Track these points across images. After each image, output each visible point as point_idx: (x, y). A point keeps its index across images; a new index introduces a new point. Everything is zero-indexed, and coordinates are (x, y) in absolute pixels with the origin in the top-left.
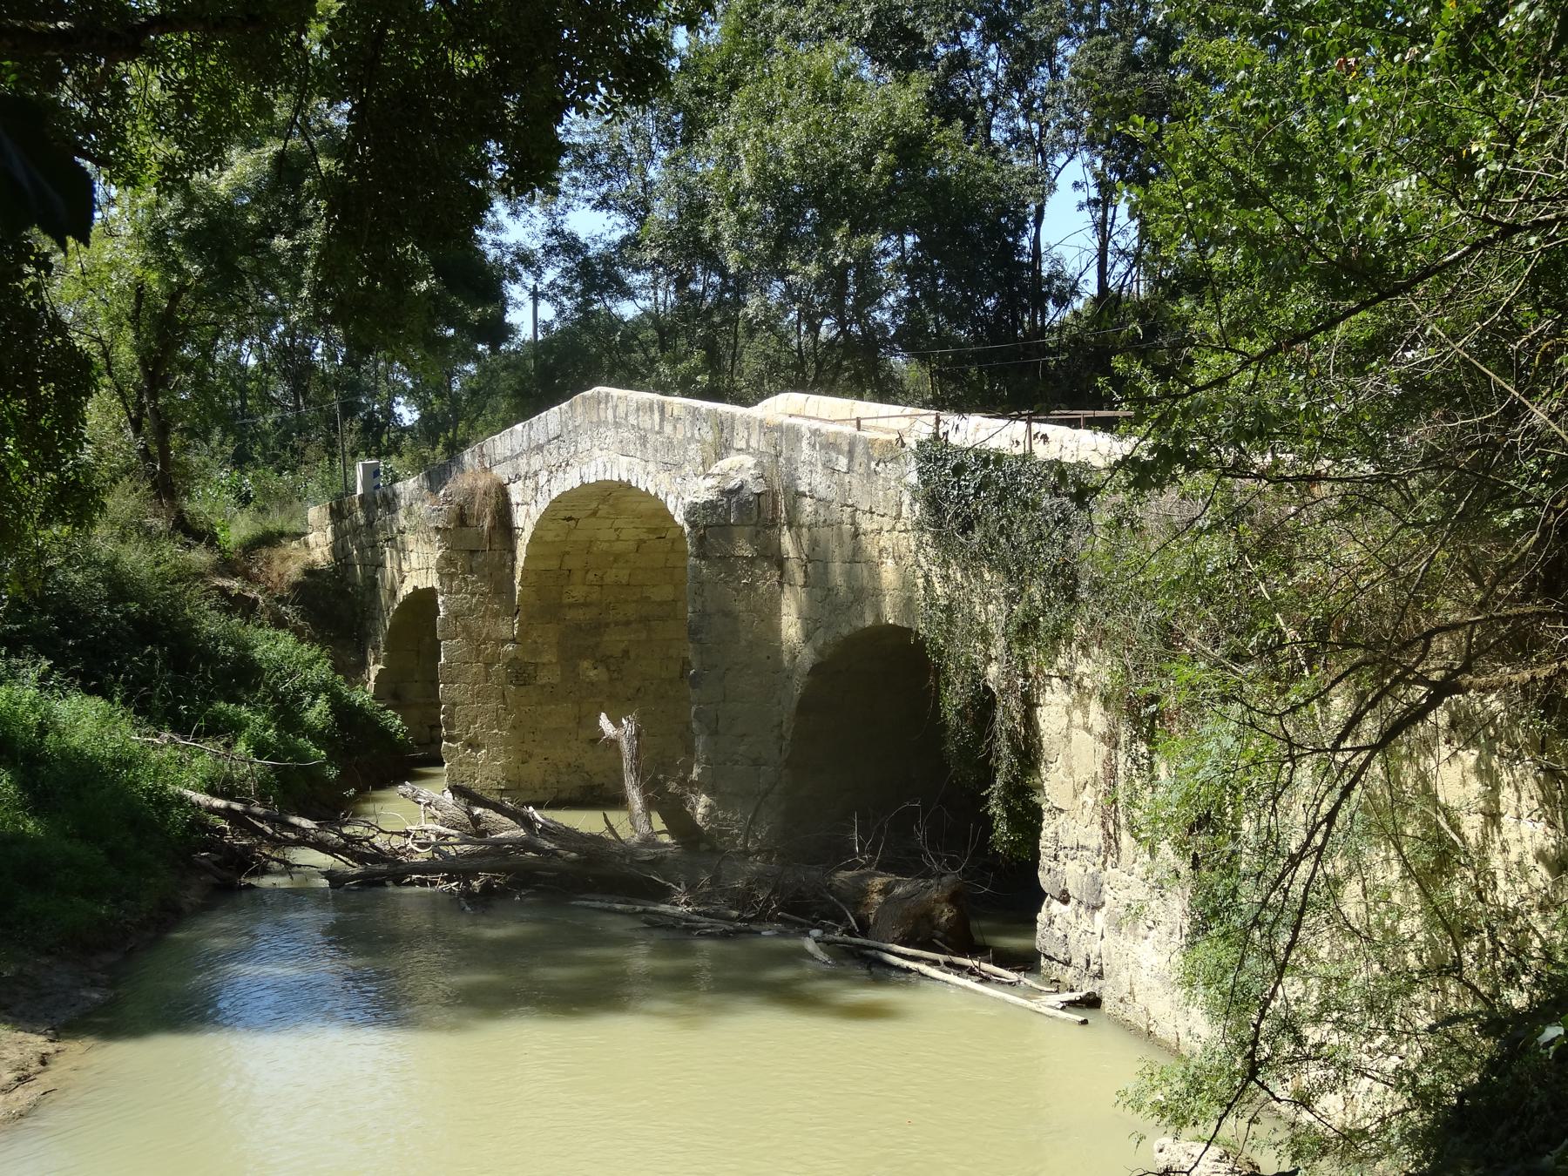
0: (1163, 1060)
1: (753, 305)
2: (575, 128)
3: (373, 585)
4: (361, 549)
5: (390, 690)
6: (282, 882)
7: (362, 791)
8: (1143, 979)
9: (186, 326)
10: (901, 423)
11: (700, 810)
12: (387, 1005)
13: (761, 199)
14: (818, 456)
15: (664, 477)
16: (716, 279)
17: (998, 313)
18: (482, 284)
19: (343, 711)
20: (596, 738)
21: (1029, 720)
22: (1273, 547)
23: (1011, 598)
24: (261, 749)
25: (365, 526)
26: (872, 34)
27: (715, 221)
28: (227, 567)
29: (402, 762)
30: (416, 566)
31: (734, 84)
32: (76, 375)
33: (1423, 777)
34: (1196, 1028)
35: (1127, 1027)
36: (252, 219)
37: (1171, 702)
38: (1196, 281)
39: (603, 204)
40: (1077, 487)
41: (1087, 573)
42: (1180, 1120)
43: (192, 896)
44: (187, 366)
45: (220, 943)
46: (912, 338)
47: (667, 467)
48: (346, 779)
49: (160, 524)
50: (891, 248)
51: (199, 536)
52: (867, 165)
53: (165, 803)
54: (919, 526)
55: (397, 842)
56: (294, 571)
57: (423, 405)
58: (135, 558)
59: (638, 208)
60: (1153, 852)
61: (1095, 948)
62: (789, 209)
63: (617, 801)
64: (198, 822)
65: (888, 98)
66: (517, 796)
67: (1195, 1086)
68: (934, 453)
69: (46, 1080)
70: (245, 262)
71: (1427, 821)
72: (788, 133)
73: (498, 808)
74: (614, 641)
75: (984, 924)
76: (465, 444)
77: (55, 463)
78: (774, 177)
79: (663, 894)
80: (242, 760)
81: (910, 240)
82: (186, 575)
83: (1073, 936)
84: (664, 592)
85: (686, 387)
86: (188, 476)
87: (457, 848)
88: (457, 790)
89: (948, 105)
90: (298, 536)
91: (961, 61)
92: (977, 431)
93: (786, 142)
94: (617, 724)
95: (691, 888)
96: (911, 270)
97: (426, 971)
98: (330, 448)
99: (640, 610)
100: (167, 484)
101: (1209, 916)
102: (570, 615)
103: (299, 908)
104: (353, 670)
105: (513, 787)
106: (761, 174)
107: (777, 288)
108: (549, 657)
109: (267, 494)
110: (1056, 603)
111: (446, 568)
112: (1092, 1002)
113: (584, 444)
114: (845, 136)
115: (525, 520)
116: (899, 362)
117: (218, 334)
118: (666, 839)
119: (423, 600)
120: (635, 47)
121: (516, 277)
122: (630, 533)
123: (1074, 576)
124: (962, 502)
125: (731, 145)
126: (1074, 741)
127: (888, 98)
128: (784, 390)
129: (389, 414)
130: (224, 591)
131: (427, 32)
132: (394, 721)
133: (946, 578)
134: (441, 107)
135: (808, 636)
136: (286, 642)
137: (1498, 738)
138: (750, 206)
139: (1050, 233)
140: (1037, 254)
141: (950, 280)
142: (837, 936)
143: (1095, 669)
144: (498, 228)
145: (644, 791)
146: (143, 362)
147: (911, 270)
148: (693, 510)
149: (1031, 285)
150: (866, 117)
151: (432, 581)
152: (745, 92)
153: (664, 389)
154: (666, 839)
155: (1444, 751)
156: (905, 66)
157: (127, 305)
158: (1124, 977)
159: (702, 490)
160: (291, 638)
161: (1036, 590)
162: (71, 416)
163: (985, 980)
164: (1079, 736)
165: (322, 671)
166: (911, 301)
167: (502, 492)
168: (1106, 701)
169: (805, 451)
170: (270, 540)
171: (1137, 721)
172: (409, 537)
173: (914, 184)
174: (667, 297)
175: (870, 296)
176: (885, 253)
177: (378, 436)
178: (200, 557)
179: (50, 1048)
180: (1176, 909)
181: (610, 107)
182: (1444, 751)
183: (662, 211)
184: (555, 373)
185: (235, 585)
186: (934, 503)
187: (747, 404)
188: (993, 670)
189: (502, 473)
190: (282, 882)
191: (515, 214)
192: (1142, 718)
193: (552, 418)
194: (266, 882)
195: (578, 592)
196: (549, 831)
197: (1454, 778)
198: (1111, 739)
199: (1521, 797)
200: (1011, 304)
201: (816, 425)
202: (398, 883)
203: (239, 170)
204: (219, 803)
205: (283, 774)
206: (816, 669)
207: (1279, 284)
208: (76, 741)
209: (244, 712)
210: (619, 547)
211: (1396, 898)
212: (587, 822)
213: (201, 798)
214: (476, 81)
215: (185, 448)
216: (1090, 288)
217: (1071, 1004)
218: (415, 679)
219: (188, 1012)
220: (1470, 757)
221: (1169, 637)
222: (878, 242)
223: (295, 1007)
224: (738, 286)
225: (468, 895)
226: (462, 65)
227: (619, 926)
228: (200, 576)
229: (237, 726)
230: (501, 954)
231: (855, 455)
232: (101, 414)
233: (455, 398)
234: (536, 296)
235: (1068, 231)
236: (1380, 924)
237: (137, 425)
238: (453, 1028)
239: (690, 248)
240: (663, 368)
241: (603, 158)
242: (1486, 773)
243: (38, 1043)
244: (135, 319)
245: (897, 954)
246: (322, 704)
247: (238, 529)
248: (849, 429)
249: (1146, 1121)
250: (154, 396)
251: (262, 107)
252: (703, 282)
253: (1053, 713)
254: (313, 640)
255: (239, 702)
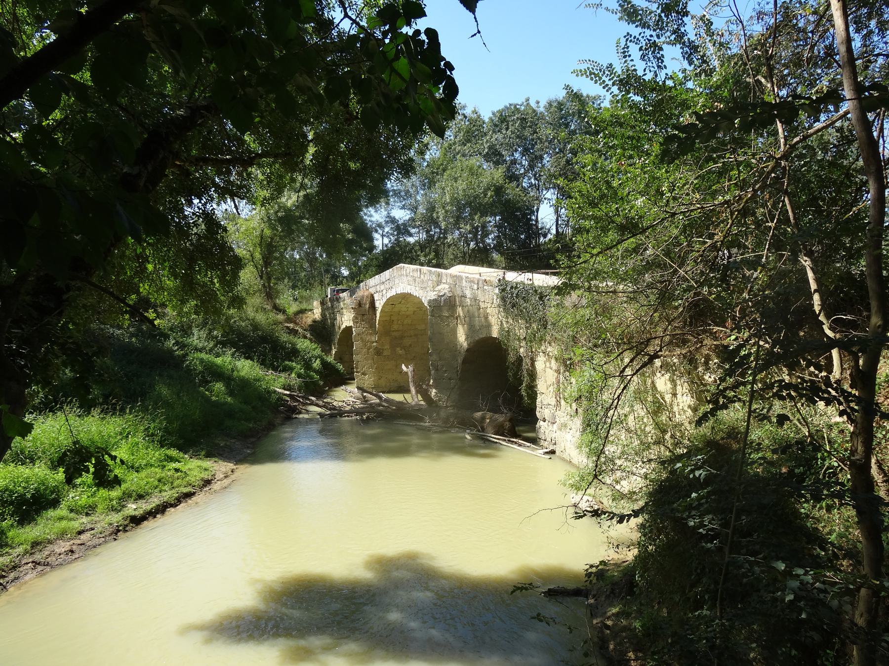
0: (573, 470)
1: (450, 238)
2: (391, 184)
3: (334, 325)
4: (330, 314)
5: (339, 358)
6: (306, 416)
7: (330, 388)
8: (568, 445)
9: (275, 247)
10: (492, 274)
11: (433, 394)
12: (339, 453)
13: (452, 205)
14: (468, 285)
15: (421, 291)
16: (438, 230)
17: (525, 240)
18: (364, 234)
19: (325, 364)
20: (401, 371)
21: (533, 365)
22: (606, 311)
23: (527, 328)
24: (299, 376)
25: (331, 308)
26: (487, 153)
27: (438, 213)
28: (289, 320)
29: (343, 379)
30: (346, 319)
31: (444, 170)
32: (238, 263)
33: (653, 382)
34: (583, 460)
35: (563, 460)
36: (297, 214)
37: (576, 359)
38: (578, 231)
39: (403, 208)
40: (541, 295)
41: (550, 320)
42: (578, 489)
43: (278, 421)
44: (276, 258)
45: (287, 435)
46: (498, 247)
47: (422, 288)
48: (325, 385)
49: (269, 307)
50: (492, 221)
51: (280, 311)
52: (485, 195)
53: (269, 392)
54: (499, 306)
55: (340, 404)
56: (309, 321)
57: (350, 269)
58: (261, 318)
59: (414, 209)
60: (571, 406)
61: (554, 435)
62: (460, 208)
63: (408, 391)
64: (280, 399)
65: (493, 174)
66: (378, 389)
67: (582, 479)
68: (503, 285)
69: (233, 477)
70: (294, 227)
71: (654, 396)
72: (461, 185)
73: (371, 393)
74: (407, 342)
75: (521, 428)
76: (362, 281)
77: (232, 291)
78: (456, 198)
79: (421, 419)
80: (294, 379)
81: (498, 218)
82: (276, 323)
83: (547, 432)
84: (422, 327)
85: (429, 264)
86: (278, 292)
87: (359, 405)
88: (359, 388)
89: (513, 177)
90: (311, 310)
91: (514, 162)
92: (512, 276)
93: (460, 188)
94: (407, 367)
95: (430, 417)
96: (499, 226)
97: (349, 442)
98: (321, 283)
99: (411, 332)
100: (270, 294)
101: (587, 424)
102: (394, 334)
103: (311, 424)
104: (328, 351)
105: (376, 387)
106: (452, 198)
107: (457, 232)
108: (387, 347)
109: (302, 297)
110: (541, 330)
111: (355, 320)
112: (553, 452)
113: (397, 281)
114: (478, 186)
115: (379, 305)
116: (496, 256)
117: (286, 249)
118: (422, 403)
119: (348, 330)
120: (405, 161)
121: (376, 231)
122: (411, 309)
123: (546, 321)
124: (513, 300)
125: (443, 189)
126: (547, 373)
127: (493, 174)
128: (459, 264)
129: (340, 272)
130: (288, 328)
131: (342, 157)
132: (340, 367)
133: (507, 322)
134: (347, 180)
135: (466, 339)
136: (307, 343)
137: (676, 370)
138: (449, 208)
139: (541, 215)
140: (537, 221)
141: (510, 230)
142: (474, 432)
143: (553, 350)
144: (371, 216)
145: (416, 388)
146: (263, 258)
147: (499, 226)
148: (430, 301)
149: (534, 231)
150: (485, 180)
151: (351, 324)
152: (448, 172)
153: (422, 265)
154: (422, 403)
155: (658, 375)
156: (497, 163)
157: (258, 240)
158: (562, 445)
159: (432, 296)
160: (308, 342)
161: (535, 326)
162: (235, 276)
163: (520, 445)
164: (548, 370)
165: (318, 352)
166: (498, 237)
167: (372, 296)
168: (556, 359)
169: (464, 283)
170: (302, 311)
171: (566, 366)
172: (344, 310)
173: (500, 201)
174: (423, 236)
175: (486, 234)
176: (490, 222)
177: (336, 278)
178: (281, 317)
179: (235, 467)
180: (577, 423)
181: (397, 179)
182: (658, 375)
183: (421, 210)
184: (389, 260)
185: (291, 325)
186: (503, 299)
187: (446, 268)
188: (522, 350)
189: (372, 291)
190: (306, 416)
191: (376, 211)
192: (568, 365)
193: (387, 274)
194: (301, 416)
195: (395, 327)
196: (387, 400)
197: (662, 383)
198: (558, 372)
199: (683, 388)
200: (529, 237)
201: (467, 275)
202: (341, 416)
203: (290, 199)
204: (288, 393)
205: (306, 383)
206: (468, 350)
207: (605, 230)
208: (242, 374)
209: (294, 364)
210: (408, 313)
211: (645, 420)
212: (398, 397)
213: (280, 391)
214: (357, 173)
215: (275, 284)
216: (554, 231)
217: (547, 453)
218: (345, 354)
219: (277, 456)
220: (667, 376)
221: (574, 339)
222: (489, 219)
223: (315, 454)
224: (446, 232)
225: (362, 420)
226: (352, 165)
227: (409, 430)
228: (281, 323)
229: (291, 369)
230: (373, 438)
231: (478, 285)
232: (248, 276)
233: (359, 268)
234: (383, 236)
235: (546, 215)
236: (640, 428)
237: (261, 277)
238: (357, 461)
239: (430, 221)
240: (422, 259)
241: (403, 194)
242: (673, 381)
243: (231, 466)
244: (260, 245)
245: (494, 438)
246: (318, 361)
247: (293, 308)
248: (478, 276)
249: (567, 489)
250: (266, 268)
251: (293, 180)
252: (434, 231)
253: (540, 364)
254: (315, 342)
255: (293, 361)
